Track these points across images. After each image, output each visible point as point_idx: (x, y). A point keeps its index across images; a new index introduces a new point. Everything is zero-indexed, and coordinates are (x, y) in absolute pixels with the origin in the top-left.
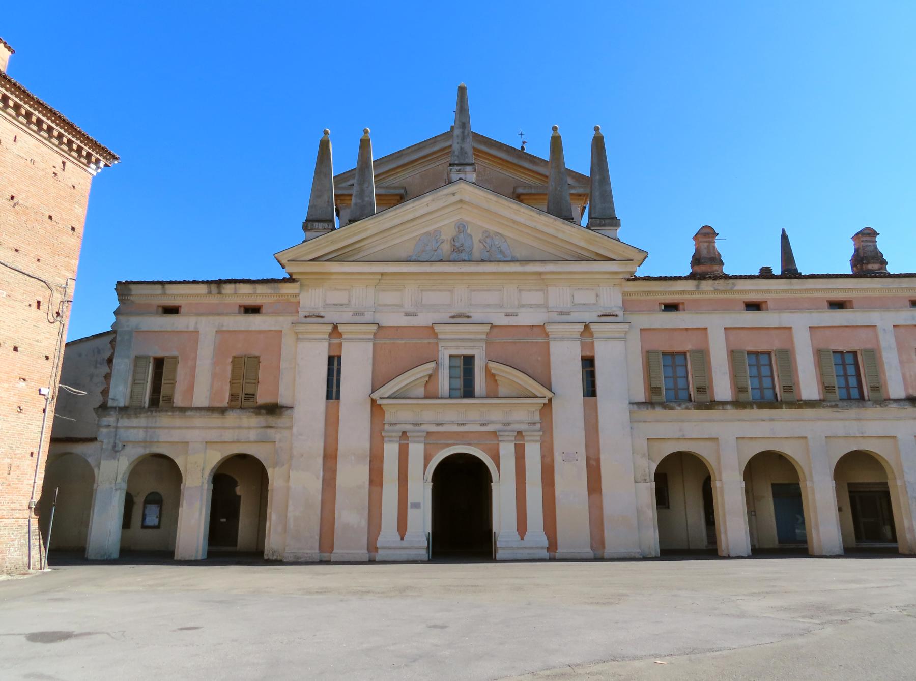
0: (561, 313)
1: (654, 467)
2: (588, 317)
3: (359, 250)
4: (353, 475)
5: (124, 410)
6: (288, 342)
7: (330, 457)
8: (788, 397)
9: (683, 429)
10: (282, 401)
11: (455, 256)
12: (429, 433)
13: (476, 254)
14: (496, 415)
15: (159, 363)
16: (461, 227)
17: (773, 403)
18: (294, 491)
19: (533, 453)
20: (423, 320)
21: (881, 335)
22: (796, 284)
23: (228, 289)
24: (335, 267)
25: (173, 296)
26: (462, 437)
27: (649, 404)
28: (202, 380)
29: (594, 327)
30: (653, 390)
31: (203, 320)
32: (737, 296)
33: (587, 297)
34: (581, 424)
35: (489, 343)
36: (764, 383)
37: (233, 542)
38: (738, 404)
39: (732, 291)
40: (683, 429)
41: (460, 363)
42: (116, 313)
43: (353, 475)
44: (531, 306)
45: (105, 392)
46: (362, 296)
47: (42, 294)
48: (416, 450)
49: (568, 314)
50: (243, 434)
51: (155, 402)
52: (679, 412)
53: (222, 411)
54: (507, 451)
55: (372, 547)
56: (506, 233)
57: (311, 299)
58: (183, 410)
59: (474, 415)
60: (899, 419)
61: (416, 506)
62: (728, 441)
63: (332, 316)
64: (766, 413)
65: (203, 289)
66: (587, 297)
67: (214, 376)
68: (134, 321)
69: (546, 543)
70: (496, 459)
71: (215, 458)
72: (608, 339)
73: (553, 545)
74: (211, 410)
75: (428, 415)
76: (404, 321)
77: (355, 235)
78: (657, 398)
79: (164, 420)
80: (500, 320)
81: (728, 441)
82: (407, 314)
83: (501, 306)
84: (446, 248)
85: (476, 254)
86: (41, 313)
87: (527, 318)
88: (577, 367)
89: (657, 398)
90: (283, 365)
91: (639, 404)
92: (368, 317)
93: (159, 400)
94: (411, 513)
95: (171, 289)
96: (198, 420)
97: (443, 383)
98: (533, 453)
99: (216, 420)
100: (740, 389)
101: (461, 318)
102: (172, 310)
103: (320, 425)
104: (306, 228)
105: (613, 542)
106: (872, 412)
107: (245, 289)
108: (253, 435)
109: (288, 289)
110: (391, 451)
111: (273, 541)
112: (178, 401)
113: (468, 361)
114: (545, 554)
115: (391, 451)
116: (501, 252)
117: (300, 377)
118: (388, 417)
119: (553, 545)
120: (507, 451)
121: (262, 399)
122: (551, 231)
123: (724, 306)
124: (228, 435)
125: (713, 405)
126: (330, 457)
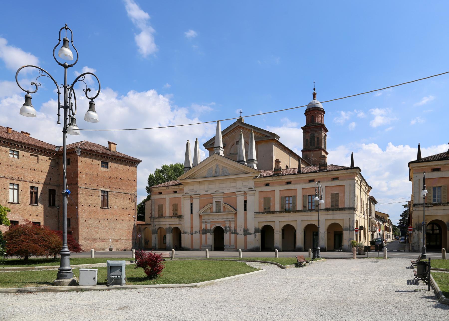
0: (240, 189)
2: (245, 189)
3: (195, 175)
6: (182, 200)
9: (267, 219)
10: (182, 215)
11: (215, 175)
12: (211, 221)
13: (221, 173)
14: (225, 217)
16: (217, 166)
17: (288, 211)
20: (209, 193)
23: (170, 187)
24: (189, 181)
28: (168, 211)
29: (246, 192)
33: (245, 184)
38: (280, 212)
44: (233, 187)
45: (151, 213)
46: (196, 187)
47: (130, 197)
49: (241, 189)
50: (174, 223)
56: (227, 167)
58: (164, 217)
59: (220, 217)
63: (191, 193)
64: (287, 214)
65: (165, 188)
67: (170, 209)
72: (250, 195)
74: (169, 217)
75: (211, 217)
76: (205, 193)
77: (15, 270)
80: (226, 191)
81: (278, 222)
82: (206, 191)
83: (226, 187)
84: (214, 172)
86: (130, 201)
87: (232, 191)
90: (182, 206)
92: (198, 193)
97: (214, 209)
99: (170, 220)
102: (161, 193)
103: (190, 220)
107: (173, 187)
109: (181, 187)
112: (164, 215)
116: (226, 172)
117: (185, 210)
121: (179, 214)
122: (236, 166)
123: (280, 184)
125: (274, 212)
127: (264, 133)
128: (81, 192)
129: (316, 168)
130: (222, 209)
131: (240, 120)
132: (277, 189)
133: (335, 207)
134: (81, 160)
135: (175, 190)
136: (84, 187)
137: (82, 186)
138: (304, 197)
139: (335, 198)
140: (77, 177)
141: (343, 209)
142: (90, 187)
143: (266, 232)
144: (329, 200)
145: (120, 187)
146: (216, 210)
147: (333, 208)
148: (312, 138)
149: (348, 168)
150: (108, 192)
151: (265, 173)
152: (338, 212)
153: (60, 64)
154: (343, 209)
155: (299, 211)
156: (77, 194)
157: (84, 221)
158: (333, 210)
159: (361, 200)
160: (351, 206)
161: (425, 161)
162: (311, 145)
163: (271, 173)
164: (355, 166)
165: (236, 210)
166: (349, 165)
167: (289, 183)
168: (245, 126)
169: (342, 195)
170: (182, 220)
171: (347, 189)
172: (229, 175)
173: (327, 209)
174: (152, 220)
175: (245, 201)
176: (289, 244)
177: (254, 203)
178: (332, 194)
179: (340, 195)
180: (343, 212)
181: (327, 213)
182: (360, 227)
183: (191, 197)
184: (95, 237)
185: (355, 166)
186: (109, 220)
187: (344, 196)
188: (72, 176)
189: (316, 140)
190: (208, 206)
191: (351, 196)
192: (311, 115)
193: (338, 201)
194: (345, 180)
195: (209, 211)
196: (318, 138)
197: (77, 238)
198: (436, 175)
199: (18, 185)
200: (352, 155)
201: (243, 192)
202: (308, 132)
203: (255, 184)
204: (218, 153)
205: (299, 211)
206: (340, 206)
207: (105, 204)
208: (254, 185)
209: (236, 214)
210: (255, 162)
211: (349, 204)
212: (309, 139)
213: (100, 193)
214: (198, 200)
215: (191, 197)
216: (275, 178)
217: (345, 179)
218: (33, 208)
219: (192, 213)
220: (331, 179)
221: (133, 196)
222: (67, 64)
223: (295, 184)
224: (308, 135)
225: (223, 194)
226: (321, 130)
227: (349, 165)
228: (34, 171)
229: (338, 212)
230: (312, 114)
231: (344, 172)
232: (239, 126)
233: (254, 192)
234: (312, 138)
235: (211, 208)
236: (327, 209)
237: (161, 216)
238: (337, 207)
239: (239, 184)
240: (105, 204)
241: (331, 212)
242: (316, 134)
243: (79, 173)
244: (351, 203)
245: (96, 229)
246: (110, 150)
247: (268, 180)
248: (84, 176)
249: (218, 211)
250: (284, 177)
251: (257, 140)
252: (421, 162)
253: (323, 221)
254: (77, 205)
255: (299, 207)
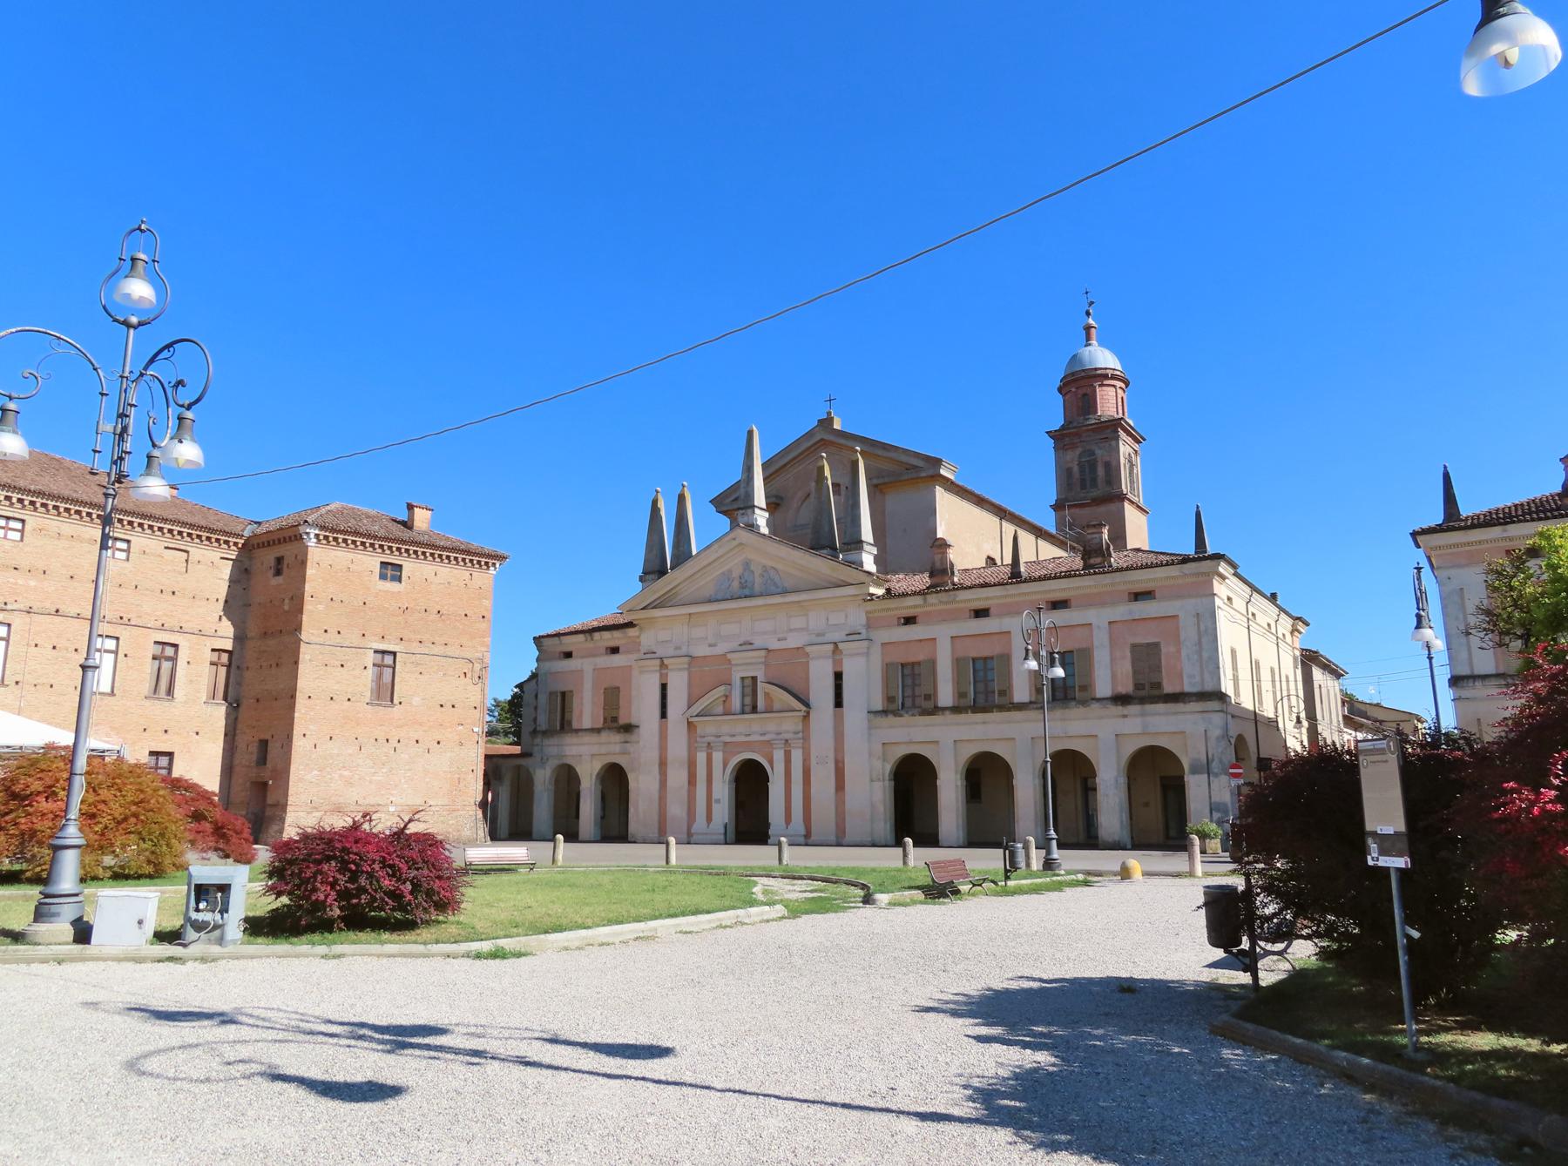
1: (888, 767)
2: (837, 636)
4: (677, 777)
5: (545, 733)
6: (635, 673)
7: (663, 764)
8: (1003, 701)
9: (913, 734)
10: (634, 721)
13: (757, 589)
14: (772, 727)
15: (563, 694)
16: (747, 565)
18: (642, 786)
19: (797, 756)
20: (719, 650)
21: (1095, 632)
22: (1024, 588)
23: (597, 635)
25: (569, 643)
26: (748, 746)
27: (885, 712)
28: (587, 711)
29: (841, 646)
30: (890, 699)
31: (586, 661)
32: (961, 605)
33: (837, 618)
34: (831, 732)
35: (766, 665)
36: (985, 689)
37: (615, 829)
38: (956, 709)
39: (953, 602)
40: (913, 734)
41: (748, 682)
42: (538, 660)
43: (677, 777)
45: (535, 720)
47: (467, 667)
48: (718, 757)
49: (822, 635)
51: (562, 727)
52: (906, 719)
53: (598, 731)
54: (779, 755)
55: (689, 834)
57: (647, 639)
60: (1101, 718)
61: (718, 801)
62: (949, 743)
63: (660, 652)
64: (980, 716)
65: (581, 637)
66: (837, 618)
68: (547, 665)
69: (803, 832)
70: (771, 763)
71: (597, 766)
72: (852, 655)
73: (808, 835)
75: (725, 729)
76: (707, 651)
78: (893, 707)
79: (569, 739)
80: (774, 645)
81: (949, 743)
84: (736, 584)
85: (757, 589)
87: (793, 642)
88: (830, 682)
89: (893, 707)
91: (876, 713)
92: (684, 651)
93: (564, 725)
94: (715, 806)
95: (566, 639)
96: (587, 738)
97: (736, 703)
98: (797, 756)
99: (593, 738)
100: (961, 695)
101: (747, 645)
102: (568, 655)
103: (656, 739)
104: (641, 579)
105: (852, 830)
106: (1076, 712)
107: (606, 635)
108: (617, 748)
109: (631, 632)
110: (701, 757)
111: (633, 827)
112: (575, 725)
113: (754, 679)
114: (802, 840)
115: (701, 757)
117: (643, 709)
118: (699, 731)
119: (808, 835)
120: (779, 755)
121: (622, 721)
124: (603, 750)
125: (936, 710)
126: (663, 764)
127: (904, 458)
128: (307, 657)
129: (922, 581)
130: (761, 704)
131: (826, 422)
132: (1098, 617)
133: (1147, 690)
134: (316, 559)
135: (613, 644)
136: (321, 640)
137: (313, 639)
138: (958, 663)
139: (1146, 657)
140: (301, 611)
141: (1177, 698)
142: (338, 640)
143: (912, 782)
144: (1126, 667)
145: (437, 640)
146: (743, 705)
147: (1142, 693)
148: (1088, 466)
149: (1186, 560)
150: (394, 654)
151: (900, 582)
152: (1161, 707)
153: (116, 320)
154: (1177, 698)
155: (1020, 707)
156: (296, 663)
157: (310, 746)
158: (1142, 701)
159: (1255, 666)
160: (1209, 687)
161: (1473, 526)
162: (1083, 487)
163: (922, 581)
164: (1210, 550)
165: (807, 705)
166: (1190, 550)
167: (981, 613)
168: (842, 441)
169: (1172, 649)
170: (633, 737)
171: (1188, 632)
172: (785, 592)
173: (1120, 699)
174: (538, 740)
175: (838, 676)
176: (989, 826)
177: (865, 685)
178: (1134, 647)
179: (1164, 650)
180: (1180, 707)
181: (1120, 710)
182: (1260, 760)
183: (663, 666)
184: (341, 800)
185: (1210, 550)
186: (393, 742)
187: (1179, 651)
188: (286, 608)
189: (1101, 471)
190: (721, 690)
191: (1205, 655)
192: (1081, 392)
193: (1158, 668)
194: (1179, 597)
195: (720, 709)
196: (1107, 465)
197: (282, 801)
198: (1060, 617)
199: (117, 639)
200: (1198, 515)
201: (831, 647)
202: (1073, 446)
203: (868, 619)
204: (752, 527)
205: (1020, 707)
206: (1168, 688)
207: (385, 692)
208: (864, 621)
209: (807, 717)
210: (866, 547)
211: (1198, 679)
212: (1076, 469)
213: (370, 658)
214: (685, 674)
215: (663, 666)
216: (932, 599)
217: (1178, 594)
218: (210, 709)
219: (664, 715)
220: (1126, 597)
221: (478, 666)
222: (134, 320)
223: (1001, 615)
224: (1072, 456)
225: (763, 653)
226: (1117, 438)
227: (1190, 550)
228: (170, 597)
229: (1161, 707)
230: (1081, 392)
231: (1173, 571)
232: (824, 438)
233: (865, 643)
234: (1088, 466)
235: (727, 697)
236: (1120, 699)
237: (564, 725)
238: (1156, 692)
239: (816, 620)
240: (385, 692)
241: (1133, 709)
242: (1099, 452)
243: (307, 597)
244: (1207, 676)
245: (346, 773)
246: (411, 528)
247: (910, 605)
248: (320, 607)
249: (748, 709)
250: (963, 595)
251: (875, 481)
252: (1460, 529)
253: (1108, 738)
254: (293, 697)
255: (946, 696)
